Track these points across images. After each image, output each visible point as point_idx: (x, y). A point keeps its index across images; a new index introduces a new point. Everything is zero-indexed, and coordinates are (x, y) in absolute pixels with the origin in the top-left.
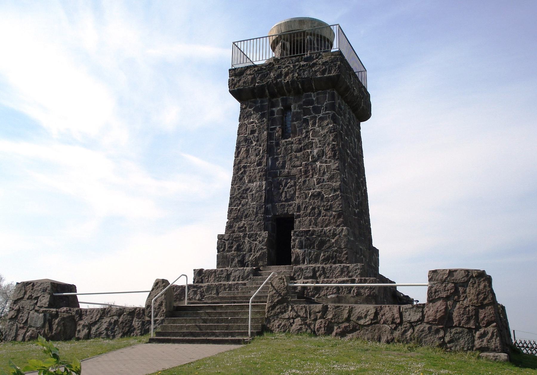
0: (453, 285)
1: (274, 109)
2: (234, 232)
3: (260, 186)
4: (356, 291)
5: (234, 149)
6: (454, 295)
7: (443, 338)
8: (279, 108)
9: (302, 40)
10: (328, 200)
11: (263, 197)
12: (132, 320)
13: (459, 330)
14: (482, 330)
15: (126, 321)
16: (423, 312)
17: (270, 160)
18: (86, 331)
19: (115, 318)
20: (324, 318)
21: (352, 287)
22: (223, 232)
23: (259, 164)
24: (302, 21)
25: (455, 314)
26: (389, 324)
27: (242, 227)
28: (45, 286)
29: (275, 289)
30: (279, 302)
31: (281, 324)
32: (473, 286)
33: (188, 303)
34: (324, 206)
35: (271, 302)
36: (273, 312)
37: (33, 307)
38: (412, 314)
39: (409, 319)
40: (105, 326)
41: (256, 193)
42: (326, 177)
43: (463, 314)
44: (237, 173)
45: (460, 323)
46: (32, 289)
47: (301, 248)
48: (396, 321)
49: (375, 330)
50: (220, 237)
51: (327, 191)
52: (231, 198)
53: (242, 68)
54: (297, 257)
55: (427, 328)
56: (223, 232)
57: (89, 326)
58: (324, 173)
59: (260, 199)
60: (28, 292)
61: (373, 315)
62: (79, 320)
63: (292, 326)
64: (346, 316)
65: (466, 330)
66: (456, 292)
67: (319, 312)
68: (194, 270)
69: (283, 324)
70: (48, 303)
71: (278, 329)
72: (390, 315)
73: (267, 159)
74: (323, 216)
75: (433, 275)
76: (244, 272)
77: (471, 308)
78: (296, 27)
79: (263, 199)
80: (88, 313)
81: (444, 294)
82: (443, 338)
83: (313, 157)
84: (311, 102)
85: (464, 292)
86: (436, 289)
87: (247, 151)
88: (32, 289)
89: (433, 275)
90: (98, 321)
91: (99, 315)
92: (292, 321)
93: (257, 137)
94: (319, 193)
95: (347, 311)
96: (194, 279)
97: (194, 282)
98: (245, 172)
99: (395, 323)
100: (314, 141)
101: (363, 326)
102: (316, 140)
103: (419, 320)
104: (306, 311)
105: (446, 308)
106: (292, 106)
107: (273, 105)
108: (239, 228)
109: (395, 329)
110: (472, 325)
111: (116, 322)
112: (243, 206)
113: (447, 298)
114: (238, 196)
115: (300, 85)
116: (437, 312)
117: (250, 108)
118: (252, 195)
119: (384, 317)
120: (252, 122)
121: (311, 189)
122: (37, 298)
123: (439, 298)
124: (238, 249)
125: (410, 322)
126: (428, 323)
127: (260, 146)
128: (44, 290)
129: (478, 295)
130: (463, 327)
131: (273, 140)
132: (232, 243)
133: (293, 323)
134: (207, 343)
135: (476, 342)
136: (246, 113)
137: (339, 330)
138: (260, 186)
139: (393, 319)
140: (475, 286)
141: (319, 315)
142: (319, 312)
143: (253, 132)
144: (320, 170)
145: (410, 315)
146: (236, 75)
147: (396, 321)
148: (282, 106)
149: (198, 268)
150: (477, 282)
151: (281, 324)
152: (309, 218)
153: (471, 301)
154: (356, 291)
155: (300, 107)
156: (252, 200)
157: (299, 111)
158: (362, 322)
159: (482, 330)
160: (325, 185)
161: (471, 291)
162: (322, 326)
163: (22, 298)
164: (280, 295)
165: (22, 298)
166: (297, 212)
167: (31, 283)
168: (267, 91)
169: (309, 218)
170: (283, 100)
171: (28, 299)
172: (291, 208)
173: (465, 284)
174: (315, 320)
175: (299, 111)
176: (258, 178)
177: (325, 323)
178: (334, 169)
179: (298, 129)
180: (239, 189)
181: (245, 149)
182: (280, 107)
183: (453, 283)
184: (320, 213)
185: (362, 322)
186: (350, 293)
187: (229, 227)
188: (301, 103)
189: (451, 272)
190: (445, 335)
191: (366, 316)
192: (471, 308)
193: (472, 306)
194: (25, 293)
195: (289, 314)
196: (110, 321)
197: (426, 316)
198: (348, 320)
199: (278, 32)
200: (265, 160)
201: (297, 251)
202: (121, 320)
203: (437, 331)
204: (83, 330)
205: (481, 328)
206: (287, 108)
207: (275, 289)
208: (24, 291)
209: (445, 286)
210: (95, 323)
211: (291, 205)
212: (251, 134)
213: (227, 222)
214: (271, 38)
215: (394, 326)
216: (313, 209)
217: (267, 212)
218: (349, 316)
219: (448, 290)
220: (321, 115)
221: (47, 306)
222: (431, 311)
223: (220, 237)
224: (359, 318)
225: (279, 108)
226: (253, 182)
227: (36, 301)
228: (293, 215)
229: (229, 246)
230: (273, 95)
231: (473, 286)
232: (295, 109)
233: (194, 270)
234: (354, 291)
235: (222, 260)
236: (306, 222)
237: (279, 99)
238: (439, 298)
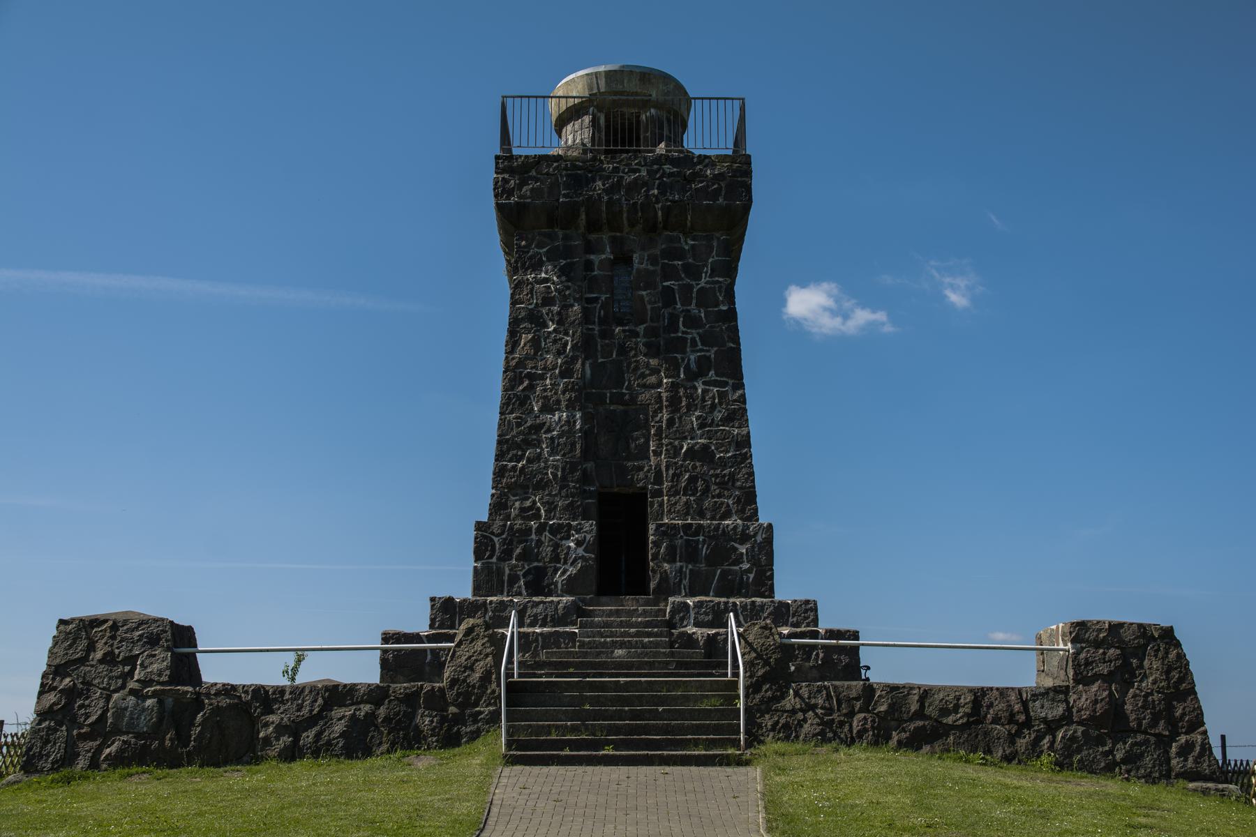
0: (1118, 652)
1: (592, 257)
2: (508, 518)
3: (570, 422)
4: (821, 655)
5: (504, 335)
6: (1124, 674)
7: (1111, 752)
8: (603, 256)
9: (635, 111)
10: (723, 463)
11: (578, 446)
12: (414, 714)
13: (1140, 738)
14: (1183, 739)
15: (397, 714)
16: (1068, 703)
17: (587, 365)
18: (286, 740)
19: (366, 708)
20: (869, 712)
21: (814, 647)
22: (485, 518)
23: (567, 372)
24: (647, 76)
25: (1128, 707)
26: (1003, 725)
27: (530, 508)
28: (154, 629)
29: (755, 651)
30: (765, 679)
31: (778, 722)
32: (1156, 656)
33: (520, 675)
34: (716, 476)
35: (751, 677)
36: (758, 697)
37: (120, 682)
38: (1047, 704)
39: (1043, 715)
40: (339, 728)
41: (560, 436)
42: (718, 416)
43: (1142, 707)
44: (512, 388)
45: (1140, 725)
46: (113, 637)
47: (672, 561)
48: (1017, 717)
49: (976, 736)
50: (479, 526)
51: (722, 445)
52: (499, 443)
53: (527, 157)
54: (665, 578)
55: (1079, 734)
56: (485, 518)
57: (294, 730)
58: (713, 407)
59: (571, 451)
60: (100, 645)
61: (970, 705)
62: (263, 714)
63: (802, 726)
64: (914, 707)
65: (1153, 739)
66: (1126, 665)
67: (857, 699)
68: (433, 599)
69: (782, 721)
70: (168, 672)
71: (771, 734)
72: (1003, 706)
73: (583, 364)
74: (713, 497)
75: (1080, 631)
76: (556, 609)
77: (1156, 697)
78: (632, 86)
79: (578, 451)
80: (287, 696)
81: (1104, 669)
82: (1111, 752)
83: (687, 368)
84: (681, 255)
85: (1141, 666)
86: (1086, 659)
87: (535, 343)
88: (113, 637)
89: (1080, 631)
90: (320, 716)
91: (320, 701)
92: (800, 716)
93: (559, 313)
94: (705, 447)
95: (916, 698)
96: (433, 621)
97: (432, 626)
98: (531, 387)
99: (1017, 722)
100: (689, 336)
101: (953, 727)
102: (694, 333)
103: (1063, 718)
104: (829, 697)
105: (1111, 694)
106: (636, 258)
107: (590, 248)
108: (522, 510)
109: (1019, 734)
110: (1161, 728)
111: (371, 716)
112: (530, 461)
113: (1108, 678)
114: (518, 440)
115: (660, 213)
116: (1096, 702)
117: (539, 246)
118: (552, 439)
119: (991, 711)
120: (546, 280)
121: (686, 438)
122: (131, 660)
123: (1096, 677)
124: (526, 556)
125: (1045, 721)
126: (1080, 723)
127: (567, 334)
128: (153, 641)
129: (1168, 672)
130: (1145, 732)
131: (594, 323)
132: (511, 542)
133: (805, 720)
134: (698, 765)
135: (1174, 762)
136: (531, 258)
137: (904, 735)
138: (568, 422)
139: (1012, 715)
140: (1160, 655)
141: (858, 705)
142: (857, 699)
143: (548, 301)
144: (704, 400)
145: (1042, 707)
146: (511, 171)
147: (1017, 717)
148: (612, 253)
149: (443, 593)
150: (1162, 647)
151: (778, 722)
152: (684, 499)
153: (1154, 682)
154: (821, 655)
155: (653, 260)
156: (552, 450)
157: (651, 268)
158: (949, 720)
159: (1183, 739)
160: (716, 432)
161: (1152, 664)
162: (869, 726)
163: (83, 660)
164: (767, 663)
165: (83, 660)
166: (654, 484)
167: (106, 621)
168: (583, 217)
169: (684, 499)
170: (613, 241)
171: (101, 661)
172: (641, 475)
173: (1140, 652)
174: (851, 714)
175: (651, 268)
176: (563, 404)
177: (873, 721)
178: (735, 401)
179: (649, 307)
180: (519, 425)
181: (530, 336)
182: (607, 254)
183: (1117, 648)
184: (706, 490)
185: (949, 720)
186: (809, 658)
187: (498, 506)
188: (625, 246)
189: (1115, 628)
190: (1113, 747)
191: (956, 708)
192: (1156, 697)
193: (1158, 692)
194: (91, 647)
195: (790, 701)
196: (354, 715)
197: (1074, 710)
198: (920, 714)
199: (591, 88)
200: (578, 366)
201: (662, 568)
202: (382, 711)
203: (1100, 741)
204: (277, 739)
205: (1179, 734)
206: (623, 259)
207: (755, 651)
208: (85, 643)
209: (1104, 653)
210: (312, 721)
211: (641, 468)
212: (544, 305)
213: (493, 495)
214: (563, 100)
215: (1014, 729)
216: (693, 480)
217: (586, 478)
218: (922, 706)
219: (1110, 661)
220: (702, 283)
221: (164, 678)
222: (1083, 700)
223: (479, 526)
224: (945, 712)
225: (603, 256)
226: (552, 412)
227: (127, 668)
228: (645, 488)
229: (503, 551)
230: (593, 226)
231: (1156, 656)
232: (639, 261)
233: (433, 599)
234: (817, 655)
235: (485, 580)
236: (678, 507)
237: (605, 237)
238: (1096, 677)
